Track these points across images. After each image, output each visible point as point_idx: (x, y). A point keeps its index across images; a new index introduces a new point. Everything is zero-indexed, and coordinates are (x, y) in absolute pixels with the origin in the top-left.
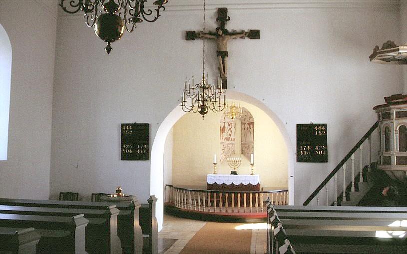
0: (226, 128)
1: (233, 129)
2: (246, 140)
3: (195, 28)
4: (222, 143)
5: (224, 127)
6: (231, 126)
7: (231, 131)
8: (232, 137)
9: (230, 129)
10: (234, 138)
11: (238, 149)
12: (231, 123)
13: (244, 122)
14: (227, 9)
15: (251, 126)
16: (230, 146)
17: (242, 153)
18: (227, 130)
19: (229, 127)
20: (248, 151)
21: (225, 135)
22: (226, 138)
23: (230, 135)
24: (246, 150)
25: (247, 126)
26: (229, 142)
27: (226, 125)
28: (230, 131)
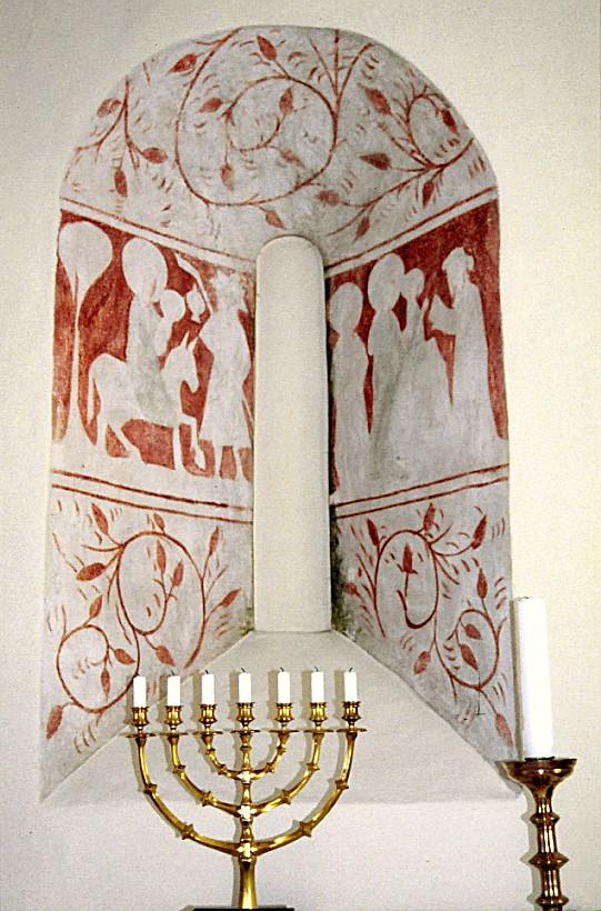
0: (139, 311)
1: (223, 335)
2: (379, 451)
3: (58, 468)
4: (71, 480)
5: (113, 288)
6: (196, 302)
7: (203, 357)
8: (220, 424)
9: (186, 327)
10: (241, 442)
11: (287, 570)
12: (204, 267)
13: (353, 251)
14: (122, 429)
15: (457, 265)
16: (191, 533)
17: (339, 619)
18: (149, 321)
19: (175, 305)
20: (423, 583)
21: (119, 386)
22: (130, 428)
23: (194, 403)
24: (390, 577)
25: (393, 282)
26: (176, 480)
27: (144, 272)
28: (184, 353)
